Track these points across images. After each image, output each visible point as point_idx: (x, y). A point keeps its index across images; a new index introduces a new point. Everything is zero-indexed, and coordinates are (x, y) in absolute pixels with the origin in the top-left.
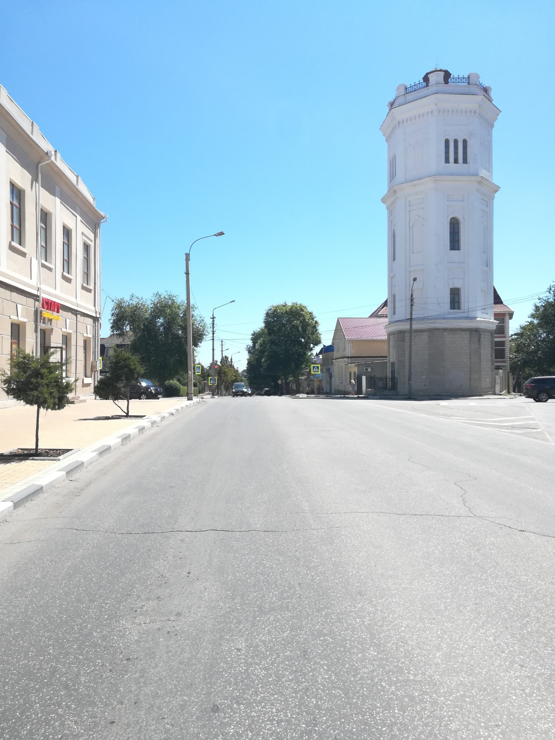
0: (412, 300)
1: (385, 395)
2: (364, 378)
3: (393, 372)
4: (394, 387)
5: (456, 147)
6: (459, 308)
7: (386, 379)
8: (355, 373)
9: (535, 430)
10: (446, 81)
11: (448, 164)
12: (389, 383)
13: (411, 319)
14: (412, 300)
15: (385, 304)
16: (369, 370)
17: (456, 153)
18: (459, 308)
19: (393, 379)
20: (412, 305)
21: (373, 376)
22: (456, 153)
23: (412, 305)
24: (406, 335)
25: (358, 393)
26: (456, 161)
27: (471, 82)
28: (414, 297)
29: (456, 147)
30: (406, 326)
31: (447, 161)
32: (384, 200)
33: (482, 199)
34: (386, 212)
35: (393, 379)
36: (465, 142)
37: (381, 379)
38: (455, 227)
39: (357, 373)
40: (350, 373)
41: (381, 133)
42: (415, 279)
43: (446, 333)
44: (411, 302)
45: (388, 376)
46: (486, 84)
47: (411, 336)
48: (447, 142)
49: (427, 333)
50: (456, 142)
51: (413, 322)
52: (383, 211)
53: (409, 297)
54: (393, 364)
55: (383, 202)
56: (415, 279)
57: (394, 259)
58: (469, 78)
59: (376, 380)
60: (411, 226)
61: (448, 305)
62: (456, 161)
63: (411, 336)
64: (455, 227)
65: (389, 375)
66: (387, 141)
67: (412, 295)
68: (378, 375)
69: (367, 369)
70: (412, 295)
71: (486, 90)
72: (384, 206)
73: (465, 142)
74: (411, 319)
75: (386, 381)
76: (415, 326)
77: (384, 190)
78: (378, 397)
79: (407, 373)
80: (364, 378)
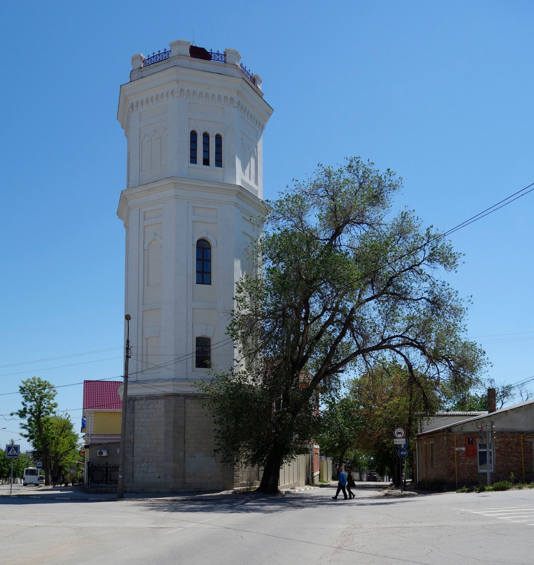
1: (312, 463)
5: (206, 144)
7: (107, 468)
16: (105, 454)
17: (206, 151)
22: (206, 151)
26: (206, 162)
27: (227, 61)
29: (206, 144)
33: (243, 217)
38: (203, 249)
43: (188, 401)
46: (253, 72)
48: (193, 135)
49: (163, 401)
50: (206, 136)
59: (109, 469)
60: (146, 248)
61: (192, 361)
62: (206, 162)
64: (203, 249)
67: (128, 341)
69: (101, 453)
70: (128, 341)
71: (254, 80)
73: (218, 138)
78: (116, 496)
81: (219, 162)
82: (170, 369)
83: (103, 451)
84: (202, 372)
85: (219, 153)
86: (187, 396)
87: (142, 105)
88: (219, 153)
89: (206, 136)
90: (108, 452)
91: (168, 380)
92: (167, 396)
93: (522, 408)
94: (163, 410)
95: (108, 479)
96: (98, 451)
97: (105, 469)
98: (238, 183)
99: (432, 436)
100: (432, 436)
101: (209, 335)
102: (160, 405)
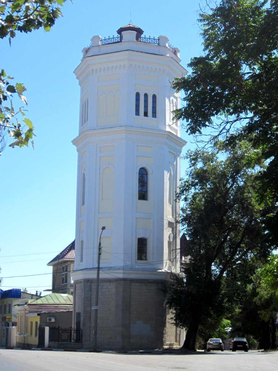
0: (100, 249)
2: (47, 329)
3: (78, 324)
4: (79, 339)
5: (146, 101)
6: (146, 260)
7: (71, 330)
8: (36, 323)
9: (171, 151)
10: (138, 37)
11: (138, 116)
12: (74, 335)
13: (99, 268)
14: (100, 249)
15: (72, 247)
16: (53, 320)
17: (146, 107)
18: (146, 260)
19: (78, 330)
20: (100, 254)
21: (57, 327)
23: (100, 254)
24: (93, 284)
25: (41, 346)
26: (146, 114)
28: (102, 245)
29: (146, 101)
30: (93, 275)
31: (137, 113)
32: (75, 142)
33: (169, 152)
34: (76, 154)
35: (78, 330)
36: (154, 97)
37: (65, 330)
39: (39, 323)
40: (32, 323)
41: (75, 76)
42: (104, 228)
44: (99, 251)
45: (73, 326)
47: (98, 286)
48: (138, 95)
49: (114, 284)
50: (146, 95)
51: (100, 272)
52: (73, 153)
53: (97, 245)
54: (78, 315)
55: (72, 142)
56: (104, 228)
57: (83, 203)
58: (159, 40)
59: (61, 331)
62: (146, 114)
63: (98, 286)
64: (143, 175)
65: (74, 326)
66: (80, 84)
67: (100, 244)
68: (63, 326)
69: (50, 320)
70: (100, 244)
72: (75, 148)
73: (154, 97)
74: (99, 268)
75: (71, 333)
76: (103, 276)
77: (75, 134)
79: (93, 324)
80: (47, 329)
81: (154, 114)
82: (118, 259)
83: (52, 318)
84: (141, 264)
85: (154, 108)
86: (132, 281)
87: (100, 72)
88: (154, 108)
89: (146, 95)
90: (55, 319)
91: (119, 269)
92: (117, 280)
93: (92, 350)
94: (114, 290)
95: (60, 338)
96: (48, 318)
97: (69, 332)
98: (168, 129)
99: (177, 152)
100: (177, 152)
101: (146, 236)
102: (112, 287)
